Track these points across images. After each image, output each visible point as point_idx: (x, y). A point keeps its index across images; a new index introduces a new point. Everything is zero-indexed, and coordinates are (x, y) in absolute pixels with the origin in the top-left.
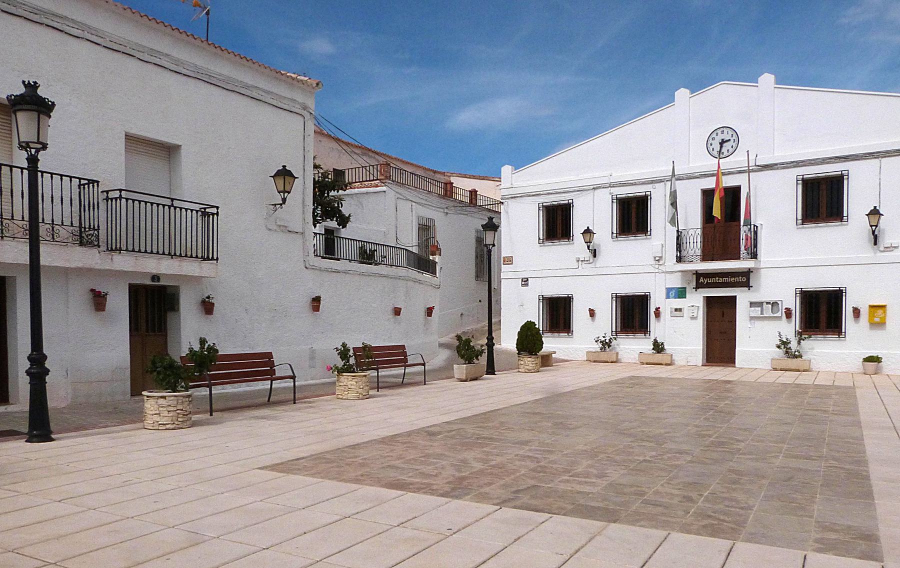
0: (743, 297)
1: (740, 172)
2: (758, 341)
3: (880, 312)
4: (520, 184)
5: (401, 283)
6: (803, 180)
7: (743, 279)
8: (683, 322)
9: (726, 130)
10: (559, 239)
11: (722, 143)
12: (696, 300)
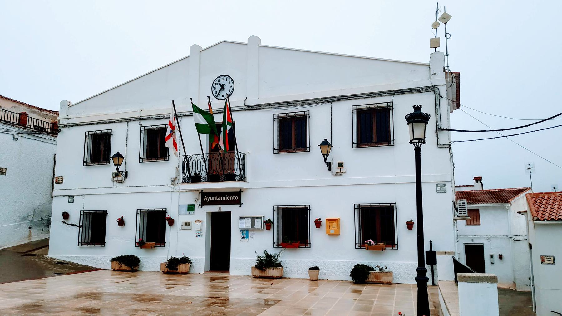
2: (245, 252)
3: (334, 224)
4: (75, 116)
7: (235, 198)
9: (225, 78)
11: (223, 87)
12: (202, 214)
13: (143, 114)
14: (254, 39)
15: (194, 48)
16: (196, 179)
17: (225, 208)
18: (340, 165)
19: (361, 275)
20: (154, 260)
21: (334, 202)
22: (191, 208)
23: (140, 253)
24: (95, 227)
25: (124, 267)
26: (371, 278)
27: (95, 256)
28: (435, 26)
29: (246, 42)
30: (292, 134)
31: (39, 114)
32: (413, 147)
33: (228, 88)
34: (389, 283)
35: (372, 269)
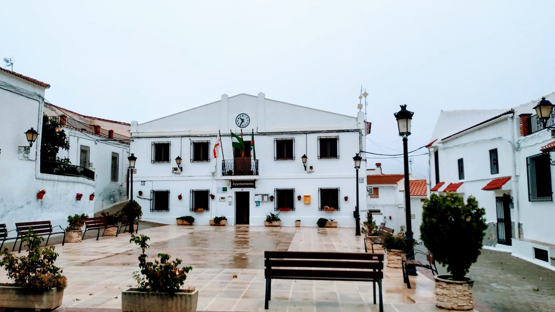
0: (251, 191)
1: (248, 135)
2: (258, 214)
3: (308, 198)
5: (133, 180)
6: (277, 140)
8: (225, 204)
10: (163, 161)
11: (243, 121)
12: (232, 193)
13: (192, 133)
14: (262, 94)
15: (224, 96)
16: (230, 173)
17: (245, 190)
18: (311, 168)
19: (322, 223)
20: (203, 219)
21: (307, 187)
22: (225, 189)
23: (193, 215)
24: (161, 200)
25: (185, 222)
26: (327, 225)
27: (162, 217)
28: (360, 98)
29: (257, 95)
30: (285, 150)
31: (83, 120)
32: (355, 169)
33: (246, 121)
34: (336, 227)
35: (327, 220)
